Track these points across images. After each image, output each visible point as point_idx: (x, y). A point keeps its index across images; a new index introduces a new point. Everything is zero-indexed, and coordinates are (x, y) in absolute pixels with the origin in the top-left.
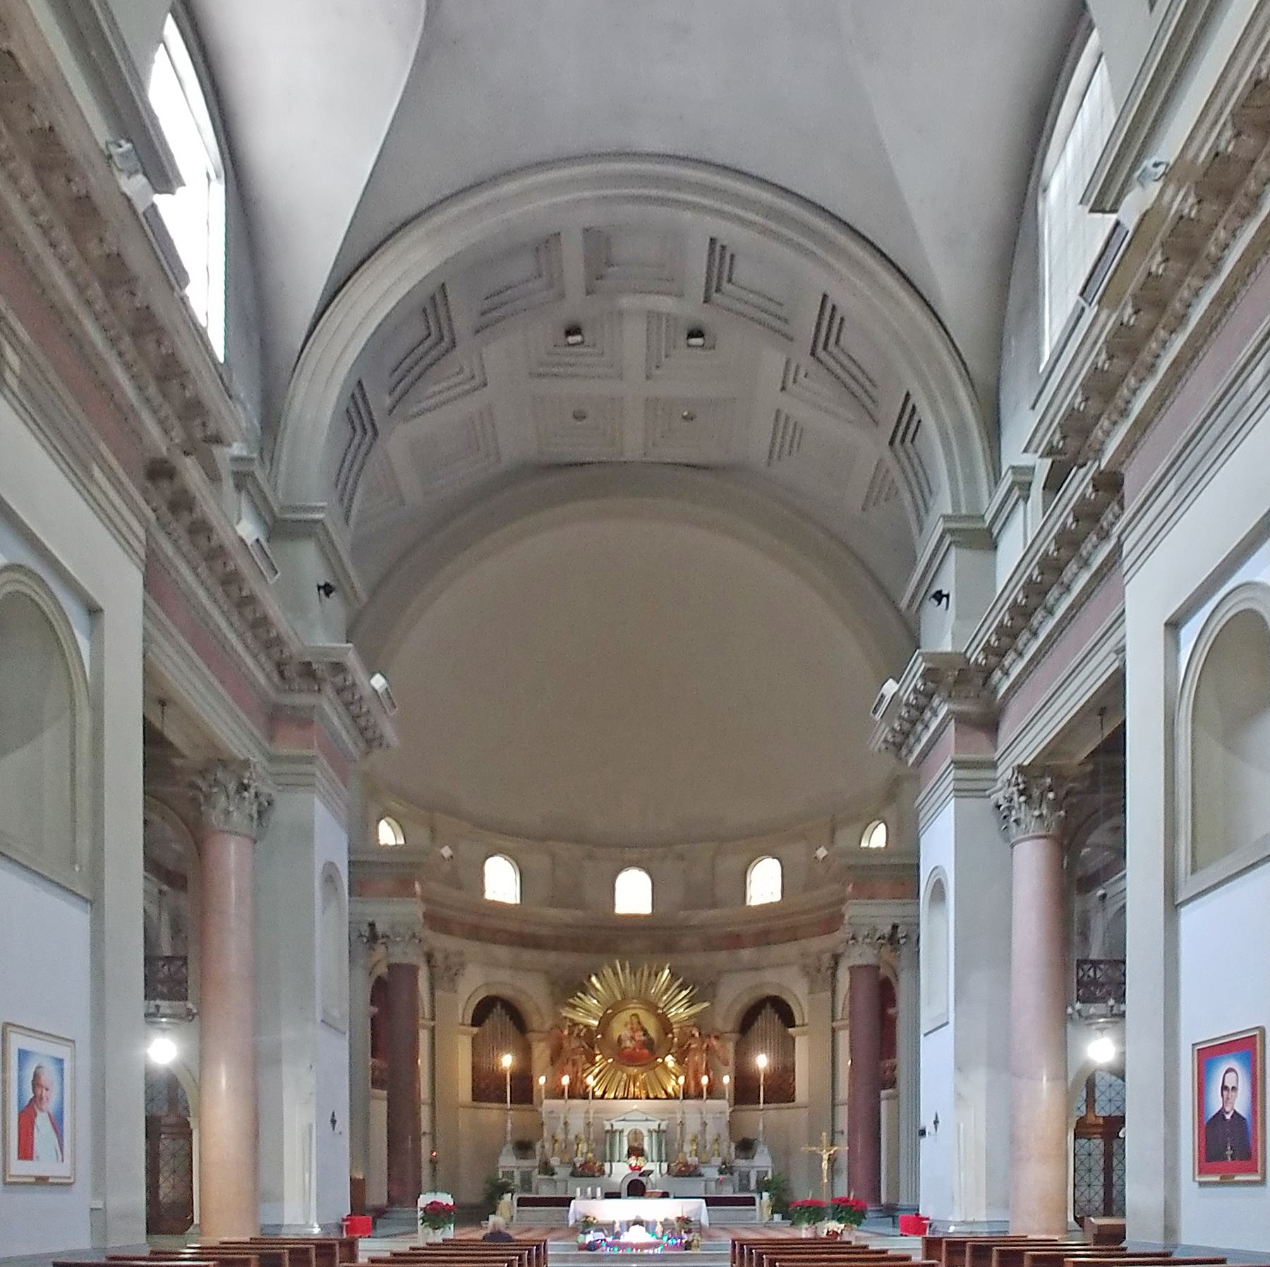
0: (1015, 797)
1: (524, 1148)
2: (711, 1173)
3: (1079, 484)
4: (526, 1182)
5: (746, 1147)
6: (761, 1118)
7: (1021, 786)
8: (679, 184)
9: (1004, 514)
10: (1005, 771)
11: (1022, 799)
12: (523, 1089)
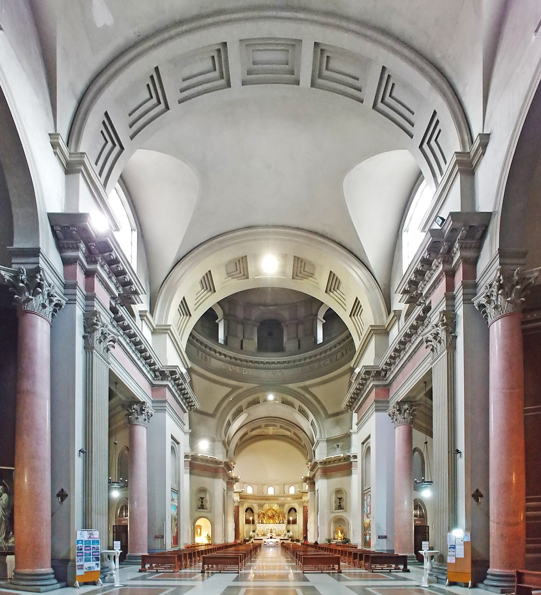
0: (396, 412)
1: (254, 531)
2: (283, 535)
3: (418, 311)
4: (254, 536)
5: (288, 531)
6: (291, 527)
7: (398, 408)
8: (276, 420)
9: (391, 325)
10: (393, 403)
11: (398, 412)
12: (253, 522)
